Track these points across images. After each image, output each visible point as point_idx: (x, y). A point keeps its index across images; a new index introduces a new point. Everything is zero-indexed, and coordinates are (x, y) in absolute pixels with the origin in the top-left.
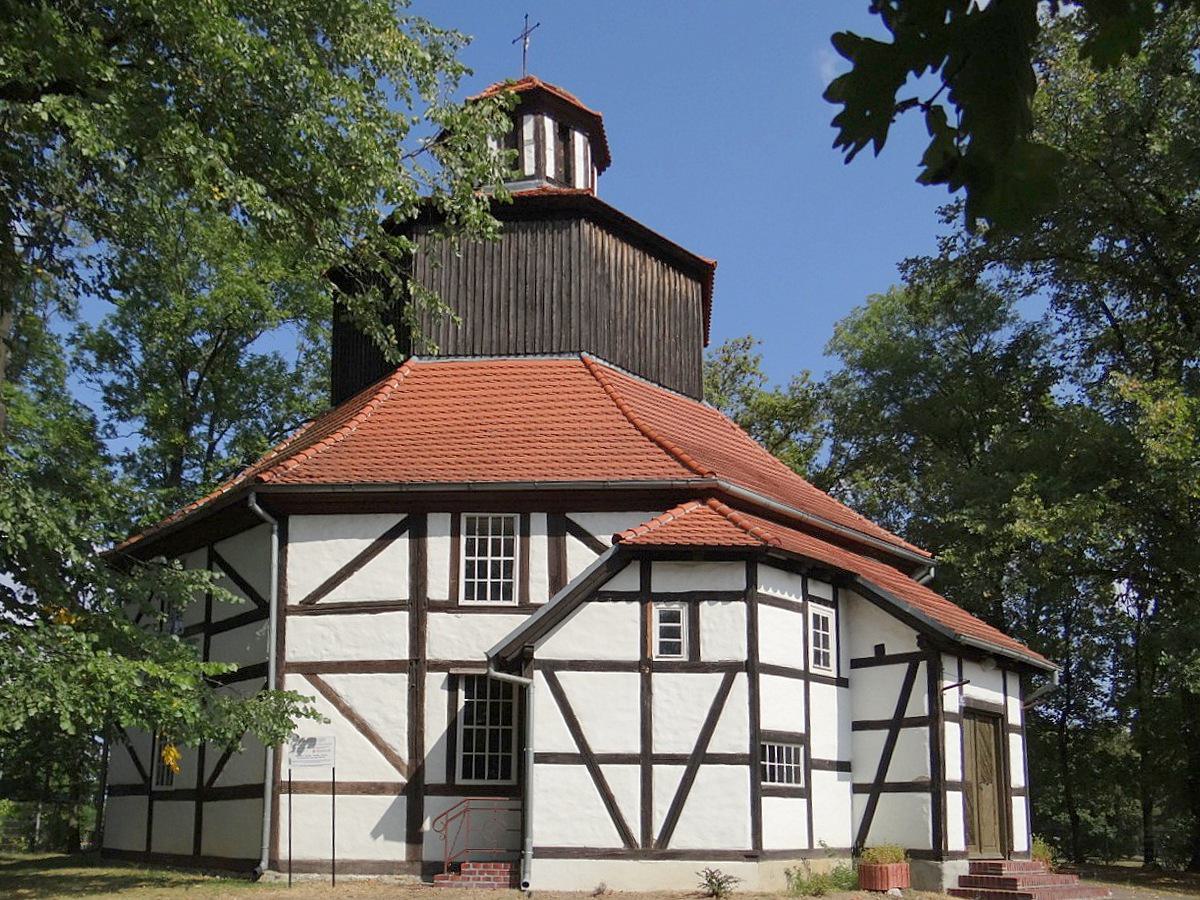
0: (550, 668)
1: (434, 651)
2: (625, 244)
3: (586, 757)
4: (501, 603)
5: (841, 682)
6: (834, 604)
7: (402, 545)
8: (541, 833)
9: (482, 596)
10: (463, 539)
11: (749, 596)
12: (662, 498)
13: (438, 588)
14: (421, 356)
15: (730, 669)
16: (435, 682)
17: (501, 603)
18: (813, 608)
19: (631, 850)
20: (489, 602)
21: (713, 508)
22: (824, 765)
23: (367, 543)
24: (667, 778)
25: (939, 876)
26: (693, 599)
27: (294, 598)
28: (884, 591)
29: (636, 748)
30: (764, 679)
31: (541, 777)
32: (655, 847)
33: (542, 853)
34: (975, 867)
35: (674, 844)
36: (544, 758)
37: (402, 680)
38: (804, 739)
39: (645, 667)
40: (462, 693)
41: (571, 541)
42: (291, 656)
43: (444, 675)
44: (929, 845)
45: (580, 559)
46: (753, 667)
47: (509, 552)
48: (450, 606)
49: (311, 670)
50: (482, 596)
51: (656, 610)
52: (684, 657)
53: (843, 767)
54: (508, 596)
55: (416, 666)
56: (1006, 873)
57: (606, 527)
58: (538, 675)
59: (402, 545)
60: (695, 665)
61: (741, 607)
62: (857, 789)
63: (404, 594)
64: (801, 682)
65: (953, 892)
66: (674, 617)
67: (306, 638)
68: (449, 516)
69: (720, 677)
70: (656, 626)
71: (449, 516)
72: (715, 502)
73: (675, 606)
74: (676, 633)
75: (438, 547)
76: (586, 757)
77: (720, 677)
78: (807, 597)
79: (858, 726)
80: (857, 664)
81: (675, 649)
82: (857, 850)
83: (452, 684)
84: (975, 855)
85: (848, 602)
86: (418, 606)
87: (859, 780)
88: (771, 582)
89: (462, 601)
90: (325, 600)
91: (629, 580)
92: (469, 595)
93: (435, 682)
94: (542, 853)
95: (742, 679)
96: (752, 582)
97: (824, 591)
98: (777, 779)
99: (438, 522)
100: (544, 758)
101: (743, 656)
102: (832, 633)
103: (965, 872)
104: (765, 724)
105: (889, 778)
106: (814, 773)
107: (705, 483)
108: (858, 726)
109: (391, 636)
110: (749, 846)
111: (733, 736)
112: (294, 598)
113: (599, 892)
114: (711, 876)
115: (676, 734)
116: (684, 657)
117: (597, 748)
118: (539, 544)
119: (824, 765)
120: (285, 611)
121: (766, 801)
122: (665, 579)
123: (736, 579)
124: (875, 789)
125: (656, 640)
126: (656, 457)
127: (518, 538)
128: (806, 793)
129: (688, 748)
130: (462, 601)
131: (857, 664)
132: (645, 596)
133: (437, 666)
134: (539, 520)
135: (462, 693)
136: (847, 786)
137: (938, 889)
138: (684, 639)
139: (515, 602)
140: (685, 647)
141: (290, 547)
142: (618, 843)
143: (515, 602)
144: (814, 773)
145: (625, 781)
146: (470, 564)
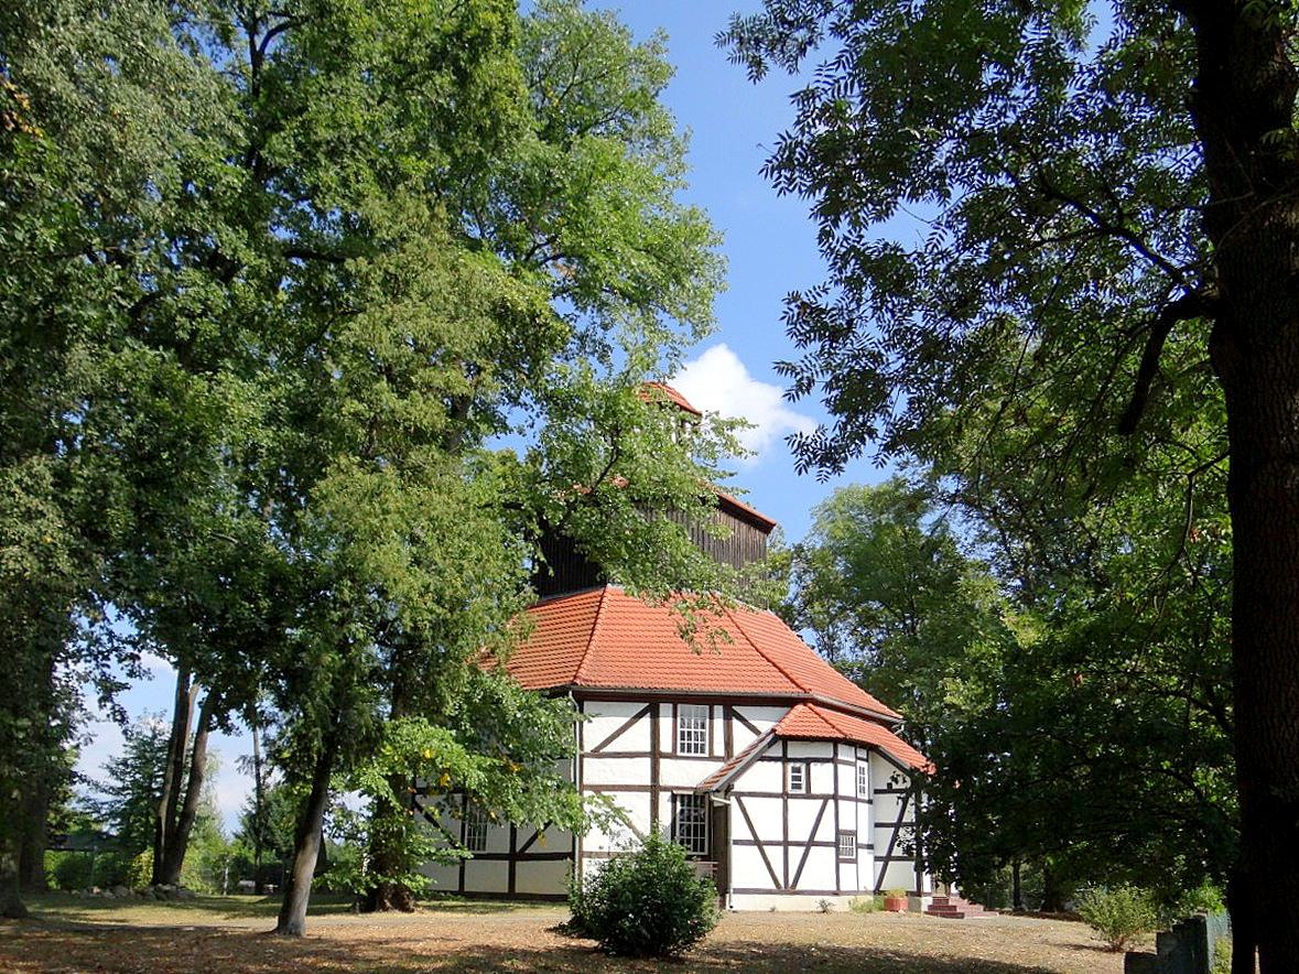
0: (739, 795)
1: (664, 781)
2: (737, 521)
3: (757, 842)
4: (699, 755)
5: (870, 802)
6: (867, 760)
7: (646, 721)
8: (737, 881)
9: (689, 751)
10: (679, 719)
11: (834, 760)
12: (789, 702)
13: (666, 745)
14: (613, 583)
15: (826, 798)
16: (664, 797)
17: (699, 755)
18: (860, 763)
19: (779, 890)
20: (693, 754)
21: (810, 708)
22: (862, 846)
23: (626, 720)
24: (796, 854)
25: (920, 904)
26: (808, 761)
27: (588, 748)
28: (894, 753)
29: (781, 839)
30: (840, 802)
31: (736, 851)
32: (789, 888)
33: (737, 891)
34: (935, 899)
35: (798, 888)
36: (737, 842)
37: (647, 796)
38: (854, 833)
39: (785, 796)
40: (678, 804)
41: (736, 723)
42: (585, 782)
43: (670, 793)
44: (915, 889)
45: (743, 738)
46: (835, 797)
47: (703, 726)
48: (672, 756)
49: (597, 789)
50: (689, 751)
51: (790, 766)
52: (803, 791)
53: (870, 847)
54: (702, 752)
55: (655, 789)
56: (950, 903)
57: (765, 721)
58: (733, 798)
59: (646, 721)
60: (809, 796)
61: (830, 766)
62: (877, 859)
63: (648, 749)
64: (854, 803)
65: (926, 913)
66: (798, 770)
67: (595, 771)
68: (671, 705)
69: (821, 802)
70: (790, 774)
71: (671, 705)
72: (811, 705)
73: (798, 765)
74: (799, 779)
75: (666, 723)
76: (757, 842)
77: (821, 802)
78: (858, 758)
79: (877, 825)
80: (877, 792)
81: (799, 787)
82: (877, 891)
83: (674, 798)
84: (934, 895)
85: (873, 756)
86: (655, 755)
87: (879, 855)
88: (845, 753)
89: (679, 753)
90: (606, 750)
91: (777, 751)
92: (682, 750)
93: (664, 797)
94: (737, 891)
95: (831, 803)
96: (836, 753)
97: (862, 753)
98: (476, 846)
99: (666, 708)
100: (737, 842)
101: (832, 792)
102: (866, 776)
103: (931, 903)
104: (841, 827)
105: (803, 849)
106: (859, 850)
107: (806, 696)
108: (877, 825)
109: (640, 771)
110: (834, 889)
111: (826, 833)
112: (588, 748)
113: (773, 910)
114: (823, 903)
115: (799, 832)
116: (803, 791)
117: (762, 838)
118: (719, 723)
119: (862, 846)
120: (582, 756)
121: (841, 865)
122: (795, 751)
123: (827, 751)
124: (888, 859)
125: (790, 782)
126: (819, 724)
127: (708, 720)
128: (855, 861)
129: (805, 838)
130: (679, 753)
131: (877, 792)
132: (785, 759)
133: (666, 789)
134: (718, 710)
135: (678, 804)
136: (871, 857)
137: (920, 912)
138: (803, 782)
139: (706, 755)
140: (804, 786)
141: (166, 727)
142: (773, 887)
143: (706, 755)
144: (859, 850)
145: (775, 854)
146: (683, 733)
